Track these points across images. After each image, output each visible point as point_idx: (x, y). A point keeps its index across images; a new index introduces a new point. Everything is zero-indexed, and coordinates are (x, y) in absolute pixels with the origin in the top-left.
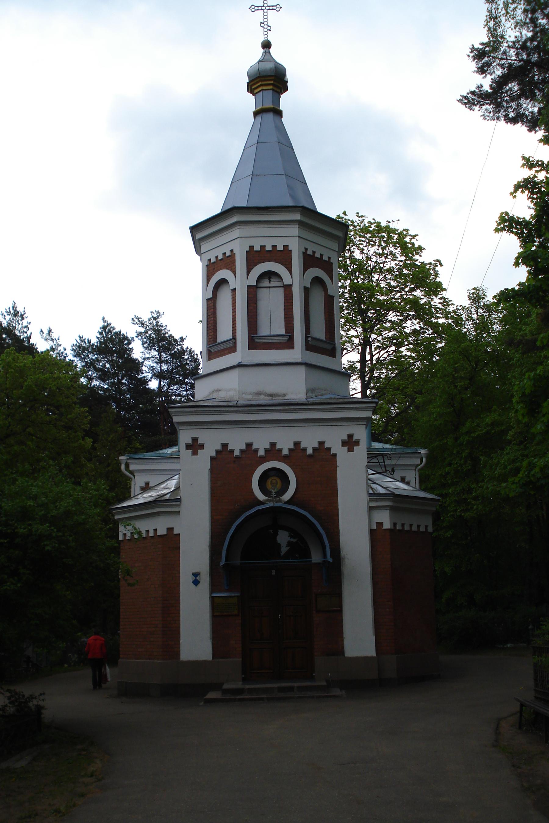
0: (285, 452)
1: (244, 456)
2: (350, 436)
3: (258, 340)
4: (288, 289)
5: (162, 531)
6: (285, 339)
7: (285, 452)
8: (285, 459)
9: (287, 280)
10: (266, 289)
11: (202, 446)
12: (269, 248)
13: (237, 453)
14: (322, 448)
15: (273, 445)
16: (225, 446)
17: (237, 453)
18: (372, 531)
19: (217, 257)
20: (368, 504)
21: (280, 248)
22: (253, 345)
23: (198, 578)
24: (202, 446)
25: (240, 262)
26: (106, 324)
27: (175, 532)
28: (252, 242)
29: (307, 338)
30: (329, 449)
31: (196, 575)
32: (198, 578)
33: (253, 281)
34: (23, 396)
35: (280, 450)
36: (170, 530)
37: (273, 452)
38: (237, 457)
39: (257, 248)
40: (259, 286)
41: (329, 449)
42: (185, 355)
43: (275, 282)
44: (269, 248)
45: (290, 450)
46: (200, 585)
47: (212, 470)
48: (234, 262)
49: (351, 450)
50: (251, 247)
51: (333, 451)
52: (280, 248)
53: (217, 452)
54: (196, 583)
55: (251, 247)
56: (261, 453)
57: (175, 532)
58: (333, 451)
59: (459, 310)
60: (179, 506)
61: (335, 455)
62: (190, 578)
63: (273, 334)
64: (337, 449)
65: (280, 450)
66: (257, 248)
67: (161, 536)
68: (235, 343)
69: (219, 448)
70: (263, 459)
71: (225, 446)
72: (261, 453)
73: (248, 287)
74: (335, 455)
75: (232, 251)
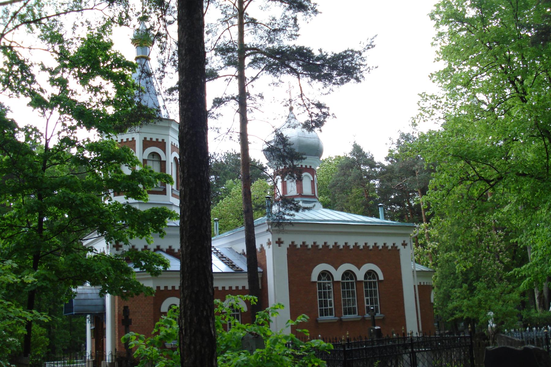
11: (282, 243)
12: (154, 140)
14: (394, 247)
19: (127, 139)
21: (160, 140)
24: (282, 243)
34: (490, 21)
39: (148, 139)
41: (396, 247)
42: (374, 185)
44: (154, 140)
48: (134, 145)
50: (145, 138)
51: (398, 248)
52: (160, 140)
55: (145, 138)
59: (509, 173)
61: (399, 250)
64: (400, 247)
66: (148, 139)
74: (399, 250)
75: (133, 138)
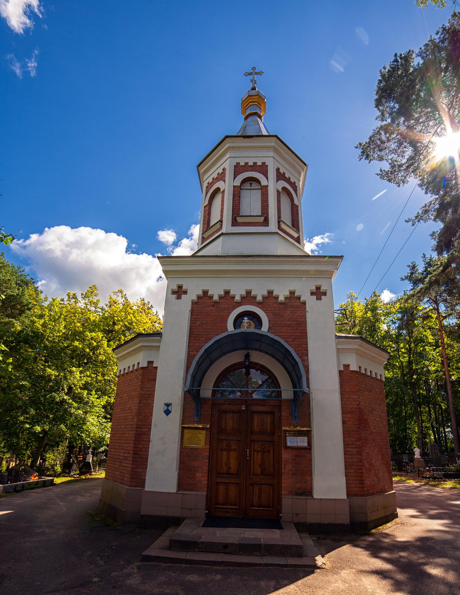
0: (259, 298)
1: (222, 301)
2: (318, 288)
3: (239, 220)
4: (264, 190)
5: (144, 364)
6: (262, 219)
7: (259, 298)
8: (259, 304)
9: (264, 182)
10: (246, 191)
11: (185, 292)
13: (216, 298)
15: (249, 293)
16: (205, 293)
17: (216, 298)
18: (340, 371)
20: (336, 346)
22: (235, 223)
23: (169, 408)
25: (229, 175)
26: (142, 271)
27: (155, 365)
28: (238, 160)
29: (279, 222)
30: (299, 298)
31: (168, 405)
32: (169, 408)
33: (238, 182)
35: (255, 297)
36: (150, 363)
37: (248, 297)
38: (216, 302)
40: (242, 188)
41: (299, 298)
43: (255, 186)
45: (264, 298)
46: (170, 415)
47: (192, 312)
49: (319, 298)
53: (199, 297)
54: (167, 412)
56: (238, 298)
57: (155, 365)
58: (302, 299)
60: (160, 341)
62: (163, 408)
63: (252, 214)
64: (306, 297)
65: (255, 297)
67: (143, 368)
68: (221, 225)
69: (200, 293)
70: (239, 304)
71: (205, 293)
72: (238, 298)
73: (234, 187)
74: (304, 303)
